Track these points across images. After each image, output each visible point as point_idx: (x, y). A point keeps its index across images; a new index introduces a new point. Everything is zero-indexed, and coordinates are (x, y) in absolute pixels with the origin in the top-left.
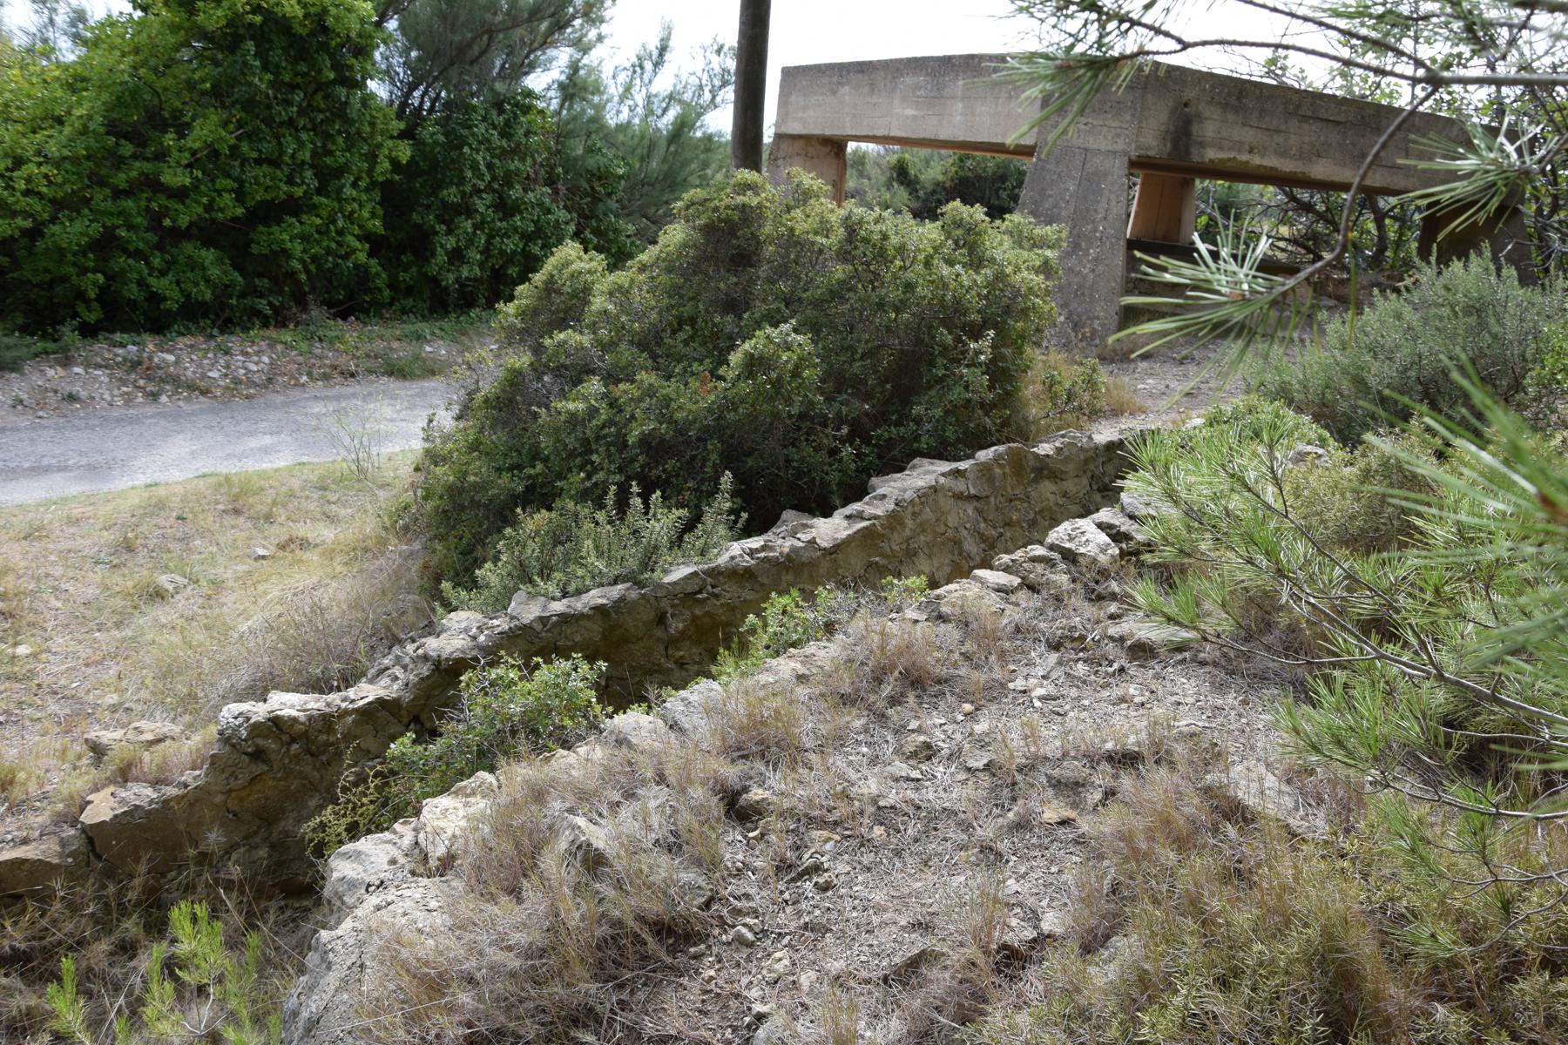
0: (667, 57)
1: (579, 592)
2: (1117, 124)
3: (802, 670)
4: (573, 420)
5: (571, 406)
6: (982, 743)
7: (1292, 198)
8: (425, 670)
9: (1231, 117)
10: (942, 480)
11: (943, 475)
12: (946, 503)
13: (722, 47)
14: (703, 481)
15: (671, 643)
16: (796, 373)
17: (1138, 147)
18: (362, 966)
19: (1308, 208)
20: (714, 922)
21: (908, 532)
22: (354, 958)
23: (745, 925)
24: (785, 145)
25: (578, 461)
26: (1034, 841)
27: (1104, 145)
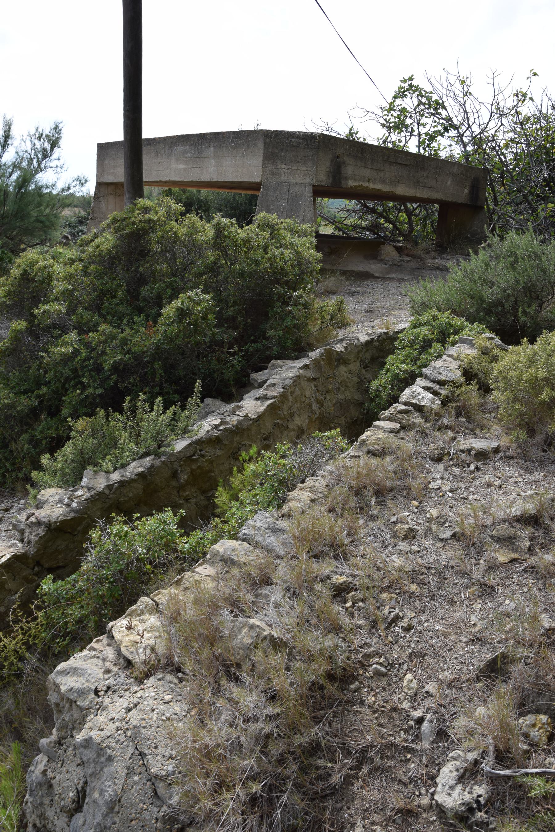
0: (10, 142)
1: (124, 466)
2: (304, 168)
3: (313, 497)
4: (66, 359)
5: (64, 350)
6: (442, 521)
7: (365, 206)
8: (41, 531)
9: (359, 163)
10: (301, 371)
11: (300, 368)
12: (304, 384)
13: (42, 134)
14: (153, 387)
15: (181, 488)
16: (205, 318)
17: (317, 181)
18: (141, 754)
19: (373, 211)
20: (358, 666)
21: (290, 404)
22: (130, 750)
23: (377, 663)
24: (103, 189)
25: (72, 383)
26: (503, 575)
27: (299, 181)
